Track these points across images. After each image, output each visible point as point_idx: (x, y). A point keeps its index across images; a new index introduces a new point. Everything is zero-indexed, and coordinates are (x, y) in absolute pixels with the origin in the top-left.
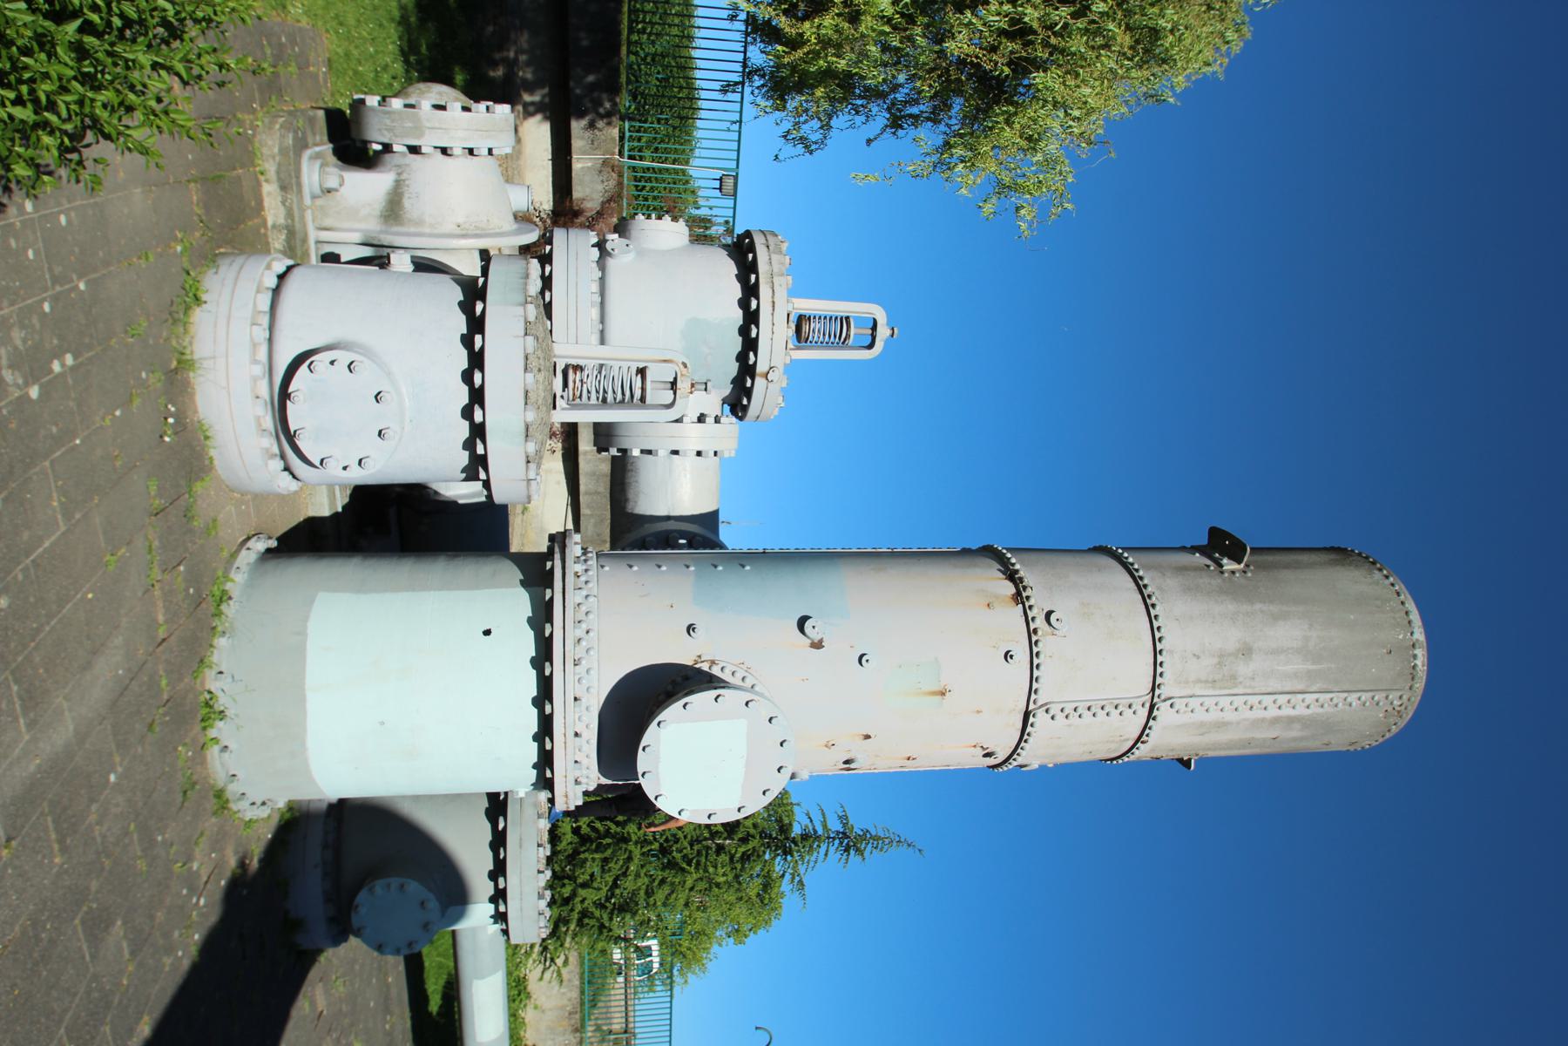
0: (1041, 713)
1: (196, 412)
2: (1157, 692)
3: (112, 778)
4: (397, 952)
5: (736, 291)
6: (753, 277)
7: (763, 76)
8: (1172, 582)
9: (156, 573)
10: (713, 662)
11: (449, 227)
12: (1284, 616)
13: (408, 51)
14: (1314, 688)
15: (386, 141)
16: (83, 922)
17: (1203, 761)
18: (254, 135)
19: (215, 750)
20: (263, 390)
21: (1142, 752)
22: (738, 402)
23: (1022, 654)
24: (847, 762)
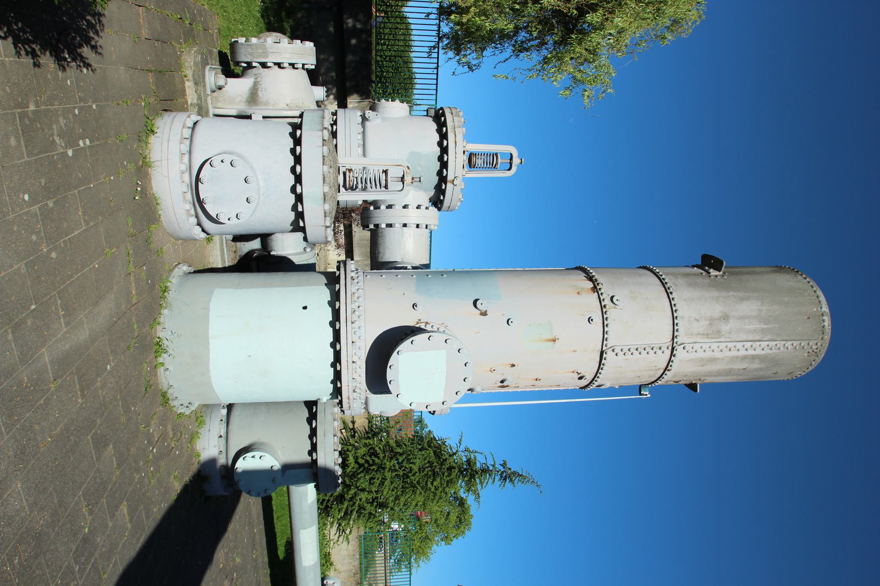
0: (609, 352)
1: (152, 189)
2: (675, 340)
3: (109, 367)
4: (258, 495)
5: (437, 138)
6: (444, 129)
7: (448, 38)
8: (681, 281)
9: (131, 268)
10: (427, 323)
11: (283, 106)
12: (747, 299)
13: (262, 25)
14: (766, 339)
15: (249, 60)
16: (92, 438)
17: (705, 385)
18: (181, 55)
19: (161, 370)
20: (186, 177)
21: (669, 377)
22: (437, 201)
23: (598, 318)
24: (502, 382)
